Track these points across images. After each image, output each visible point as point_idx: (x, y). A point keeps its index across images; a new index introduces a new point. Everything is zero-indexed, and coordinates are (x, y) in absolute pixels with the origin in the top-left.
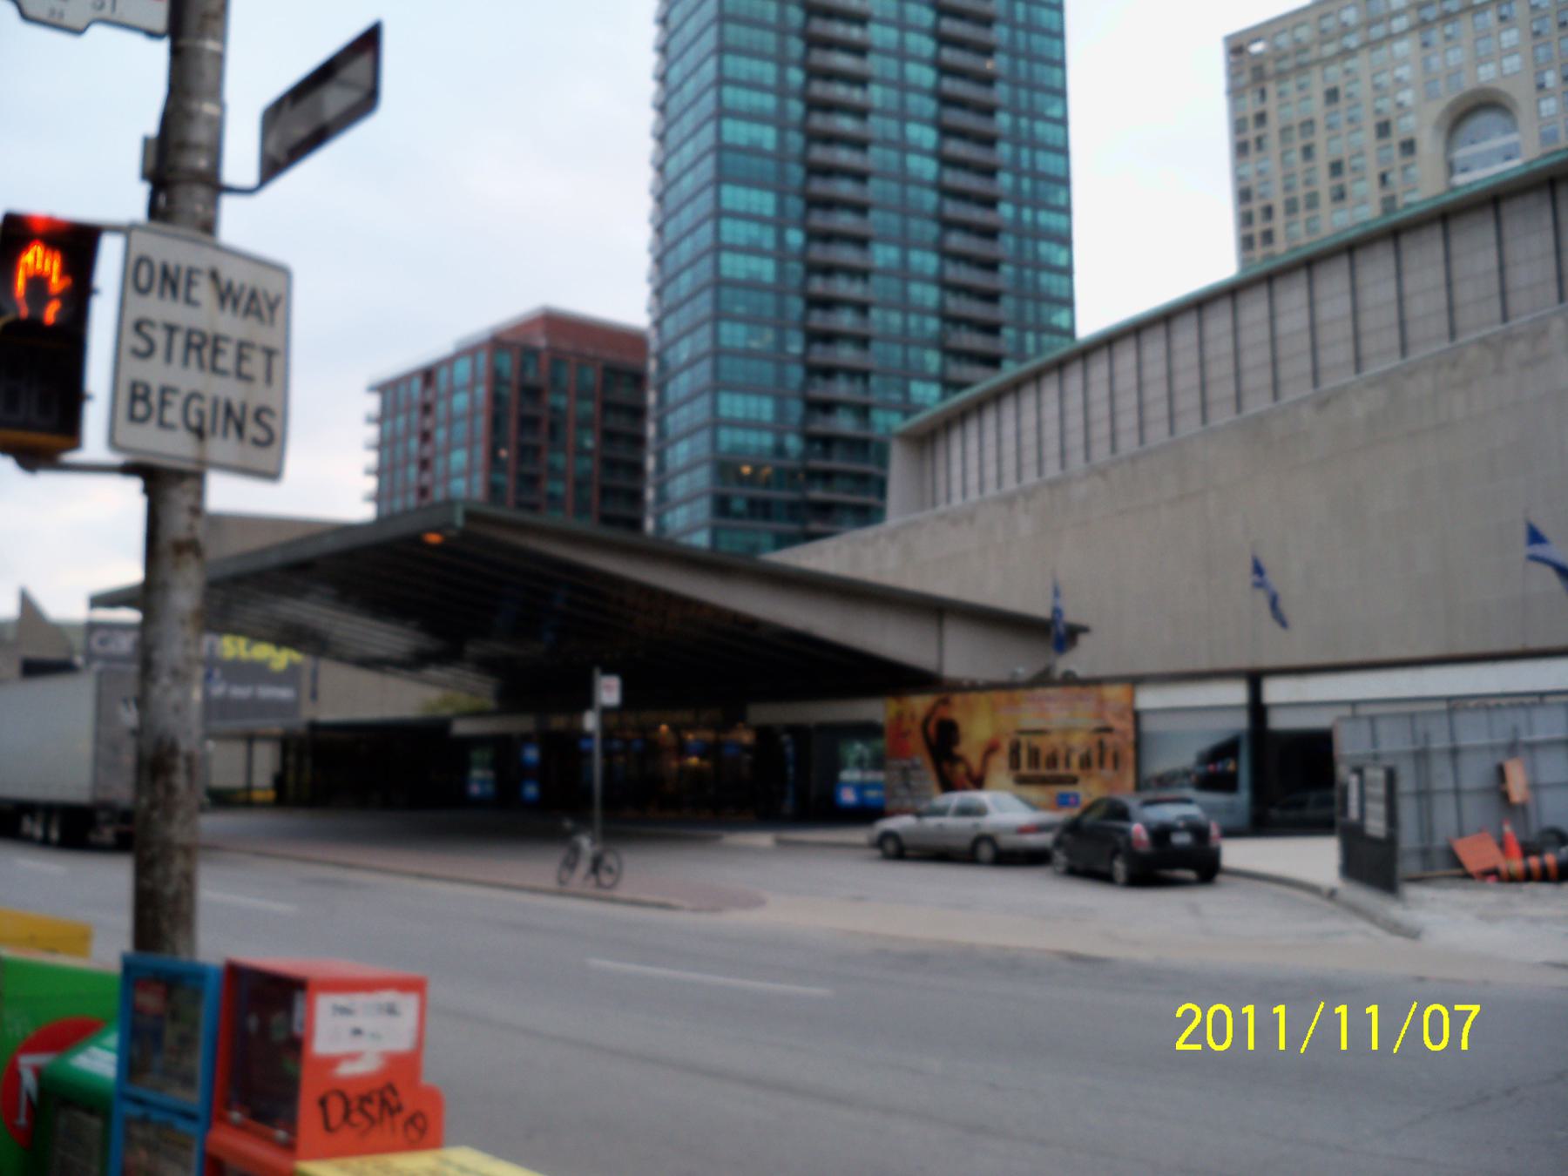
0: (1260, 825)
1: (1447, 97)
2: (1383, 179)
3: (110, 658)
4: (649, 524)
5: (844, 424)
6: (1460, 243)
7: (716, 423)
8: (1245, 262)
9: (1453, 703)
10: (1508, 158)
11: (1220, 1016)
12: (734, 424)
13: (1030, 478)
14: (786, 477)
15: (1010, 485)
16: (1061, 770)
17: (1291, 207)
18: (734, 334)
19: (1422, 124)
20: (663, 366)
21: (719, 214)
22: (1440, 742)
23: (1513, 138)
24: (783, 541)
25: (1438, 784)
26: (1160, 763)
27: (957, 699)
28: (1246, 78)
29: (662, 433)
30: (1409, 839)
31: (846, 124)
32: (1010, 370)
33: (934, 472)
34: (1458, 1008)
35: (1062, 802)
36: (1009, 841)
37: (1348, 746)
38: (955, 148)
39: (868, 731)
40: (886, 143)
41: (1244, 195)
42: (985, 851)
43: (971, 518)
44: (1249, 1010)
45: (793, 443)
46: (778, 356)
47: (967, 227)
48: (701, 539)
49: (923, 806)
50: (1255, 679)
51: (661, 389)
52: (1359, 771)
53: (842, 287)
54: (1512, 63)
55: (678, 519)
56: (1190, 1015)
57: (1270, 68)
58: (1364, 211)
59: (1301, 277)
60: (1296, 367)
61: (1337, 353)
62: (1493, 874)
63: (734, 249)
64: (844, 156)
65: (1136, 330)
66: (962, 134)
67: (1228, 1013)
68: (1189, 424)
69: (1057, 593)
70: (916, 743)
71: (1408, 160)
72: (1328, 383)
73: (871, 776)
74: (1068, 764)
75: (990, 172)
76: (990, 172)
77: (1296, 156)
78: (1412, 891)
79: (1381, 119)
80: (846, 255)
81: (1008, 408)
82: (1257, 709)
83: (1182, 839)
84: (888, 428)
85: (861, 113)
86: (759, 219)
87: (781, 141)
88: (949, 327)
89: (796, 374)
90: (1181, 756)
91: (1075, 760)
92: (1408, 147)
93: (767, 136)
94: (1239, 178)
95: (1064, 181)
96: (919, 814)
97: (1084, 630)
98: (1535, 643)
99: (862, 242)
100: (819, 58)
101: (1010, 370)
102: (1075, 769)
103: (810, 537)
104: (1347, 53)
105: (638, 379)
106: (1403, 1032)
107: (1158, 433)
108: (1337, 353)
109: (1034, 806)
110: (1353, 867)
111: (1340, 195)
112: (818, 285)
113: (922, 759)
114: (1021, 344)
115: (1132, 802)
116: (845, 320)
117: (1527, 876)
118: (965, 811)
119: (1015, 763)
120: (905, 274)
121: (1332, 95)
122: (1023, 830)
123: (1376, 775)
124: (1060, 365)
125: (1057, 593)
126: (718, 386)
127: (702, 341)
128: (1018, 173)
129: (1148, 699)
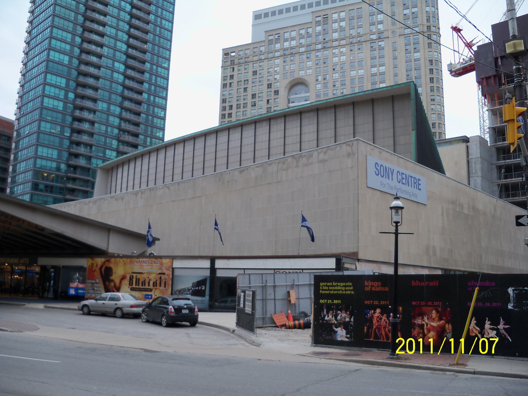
0: (211, 308)
2: (268, 101)
3: (510, 41)
4: (8, 190)
5: (82, 162)
6: (305, 122)
7: (36, 157)
8: (221, 122)
9: (276, 271)
10: (306, 100)
11: (411, 342)
12: (42, 158)
13: (144, 186)
14: (58, 178)
15: (137, 188)
16: (147, 287)
17: (238, 106)
18: (46, 127)
19: (282, 85)
20: (18, 135)
21: (45, 84)
22: (270, 283)
23: (308, 94)
24: (56, 201)
25: (269, 297)
26: (179, 286)
27: (113, 260)
28: (229, 63)
29: (16, 159)
30: (258, 314)
31: (94, 59)
32: (141, 149)
34: (491, 339)
35: (146, 297)
36: (127, 310)
37: (241, 283)
38: (130, 72)
39: (81, 269)
40: (107, 68)
41: (223, 101)
42: (119, 313)
43: (122, 199)
44: (421, 340)
45: (63, 166)
46: (61, 136)
47: (131, 100)
48: (27, 198)
49: (98, 297)
50: (213, 260)
51: (17, 143)
52: (244, 292)
53: (86, 115)
54: (309, 72)
55: (19, 190)
56: (401, 342)
57: (236, 61)
58: (261, 110)
59: (239, 129)
60: (234, 158)
61: (248, 155)
62: (284, 326)
63: (49, 97)
64: (92, 70)
65: (183, 141)
66: (133, 69)
67: (414, 341)
68: (198, 173)
69: (150, 227)
70: (97, 274)
71: (276, 97)
72: (244, 164)
73: (81, 286)
74: (149, 285)
75: (141, 83)
76: (141, 83)
77: (242, 90)
78: (258, 331)
79: (270, 82)
80: (89, 104)
81: (146, 160)
82: (213, 270)
83: (185, 311)
84: (97, 165)
85: (100, 56)
86: (59, 88)
87: (70, 61)
88: (121, 132)
89: (67, 143)
90: (187, 284)
91: (151, 283)
92: (277, 92)
93: (66, 59)
94: (222, 95)
95: (166, 89)
96: (96, 300)
97: (158, 239)
98: (301, 254)
99: (95, 100)
100: (87, 35)
101: (141, 149)
102: (151, 286)
103: (67, 200)
104: (261, 60)
105: (9, 138)
106: (472, 347)
107: (187, 175)
108: (248, 155)
109: (136, 298)
110: (240, 323)
111: (254, 105)
112: (77, 113)
113: (99, 280)
114: (145, 141)
115: (170, 299)
116: (86, 126)
117: (295, 327)
118: (112, 299)
119: (131, 283)
120: (108, 113)
121: (255, 73)
122: (132, 306)
123: (249, 293)
124: (157, 150)
125: (150, 227)
126: (38, 144)
127: (34, 127)
128: (150, 84)
129: (177, 264)
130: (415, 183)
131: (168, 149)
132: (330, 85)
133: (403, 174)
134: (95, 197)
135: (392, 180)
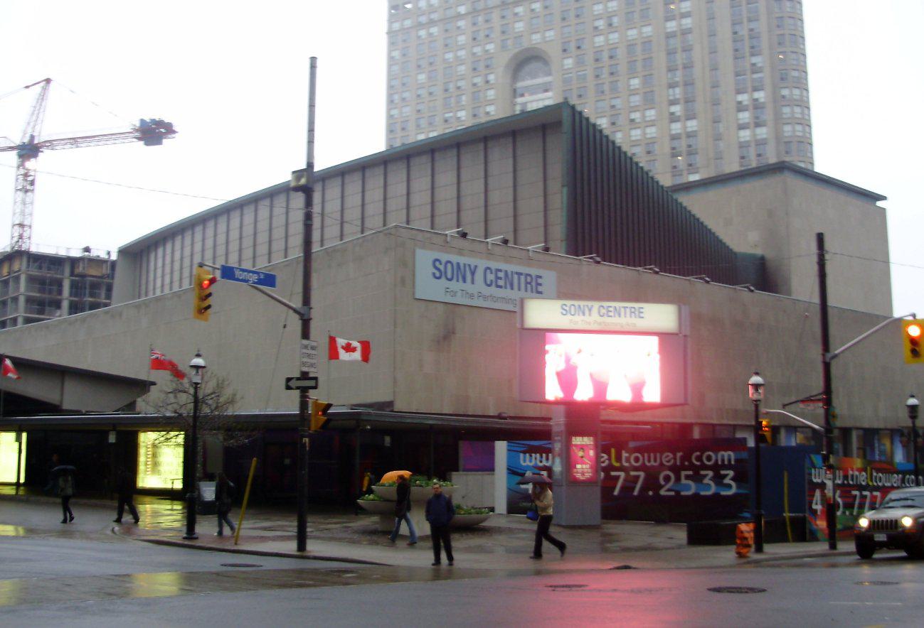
1: (513, 50)
6: (440, 165)
23: (549, 79)
33: (141, 267)
43: (121, 315)
54: (550, 34)
130: (527, 283)
131: (329, 183)
132: (589, 59)
133: (500, 271)
134: (116, 304)
135: (473, 283)
